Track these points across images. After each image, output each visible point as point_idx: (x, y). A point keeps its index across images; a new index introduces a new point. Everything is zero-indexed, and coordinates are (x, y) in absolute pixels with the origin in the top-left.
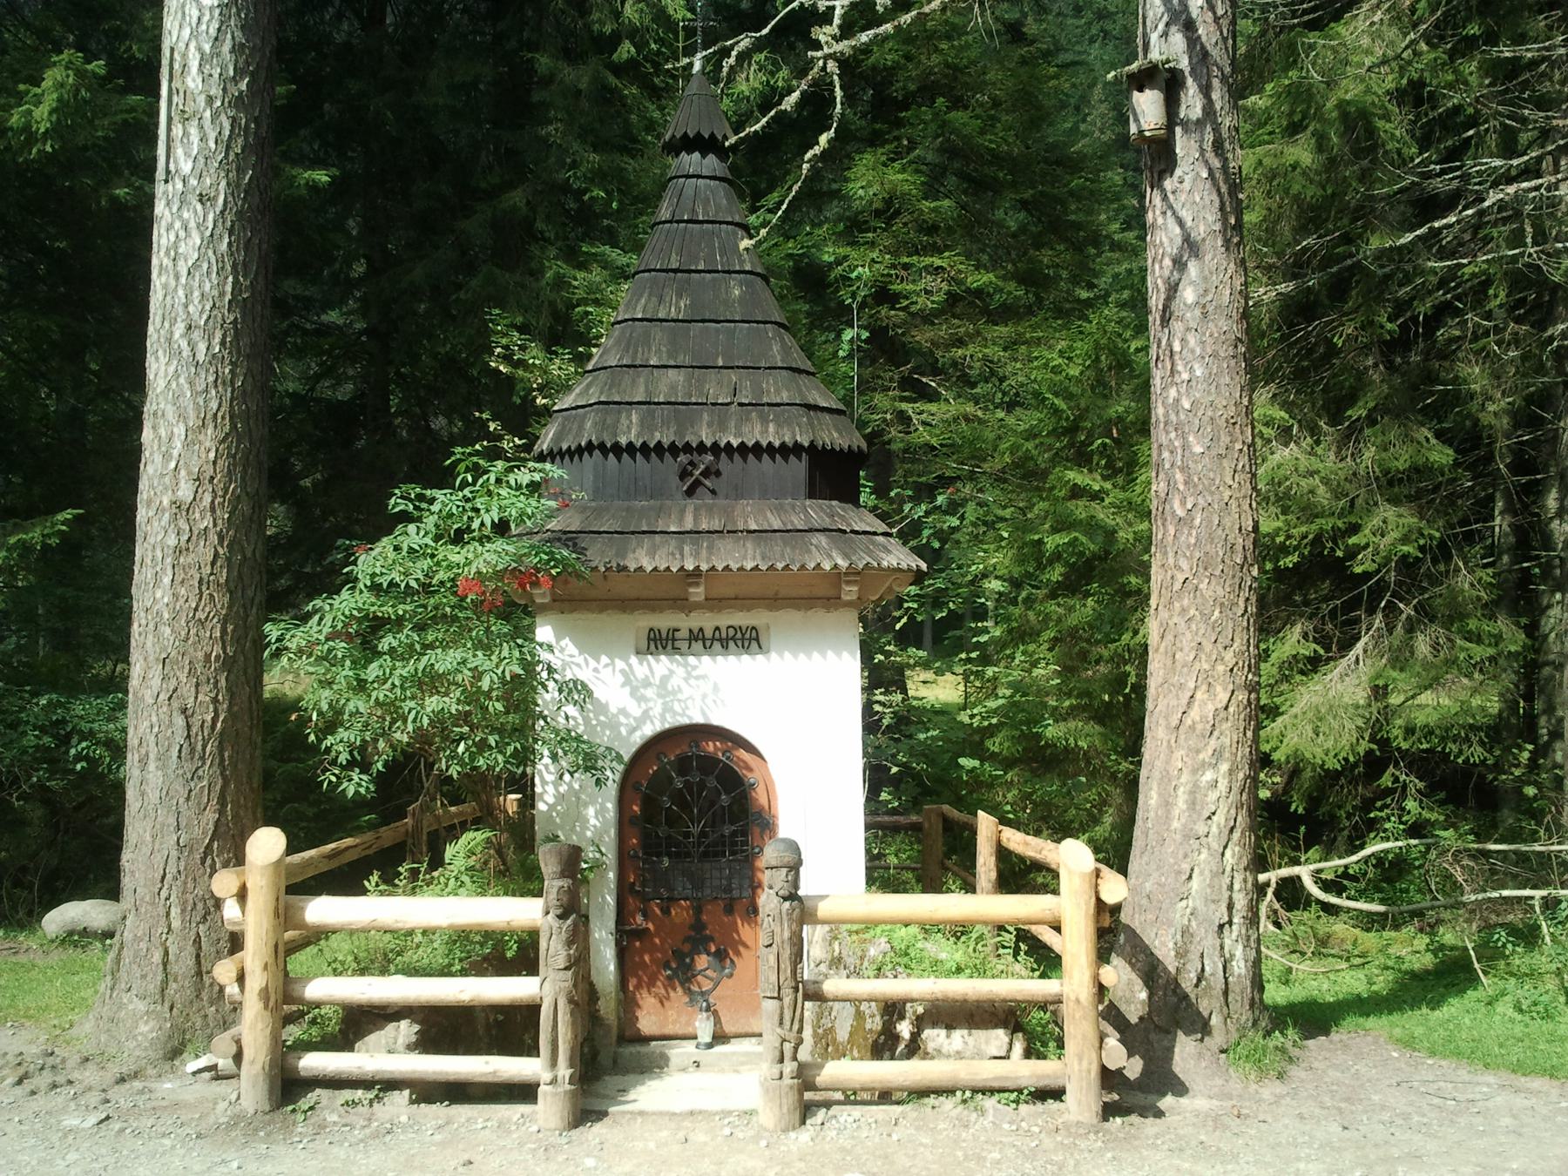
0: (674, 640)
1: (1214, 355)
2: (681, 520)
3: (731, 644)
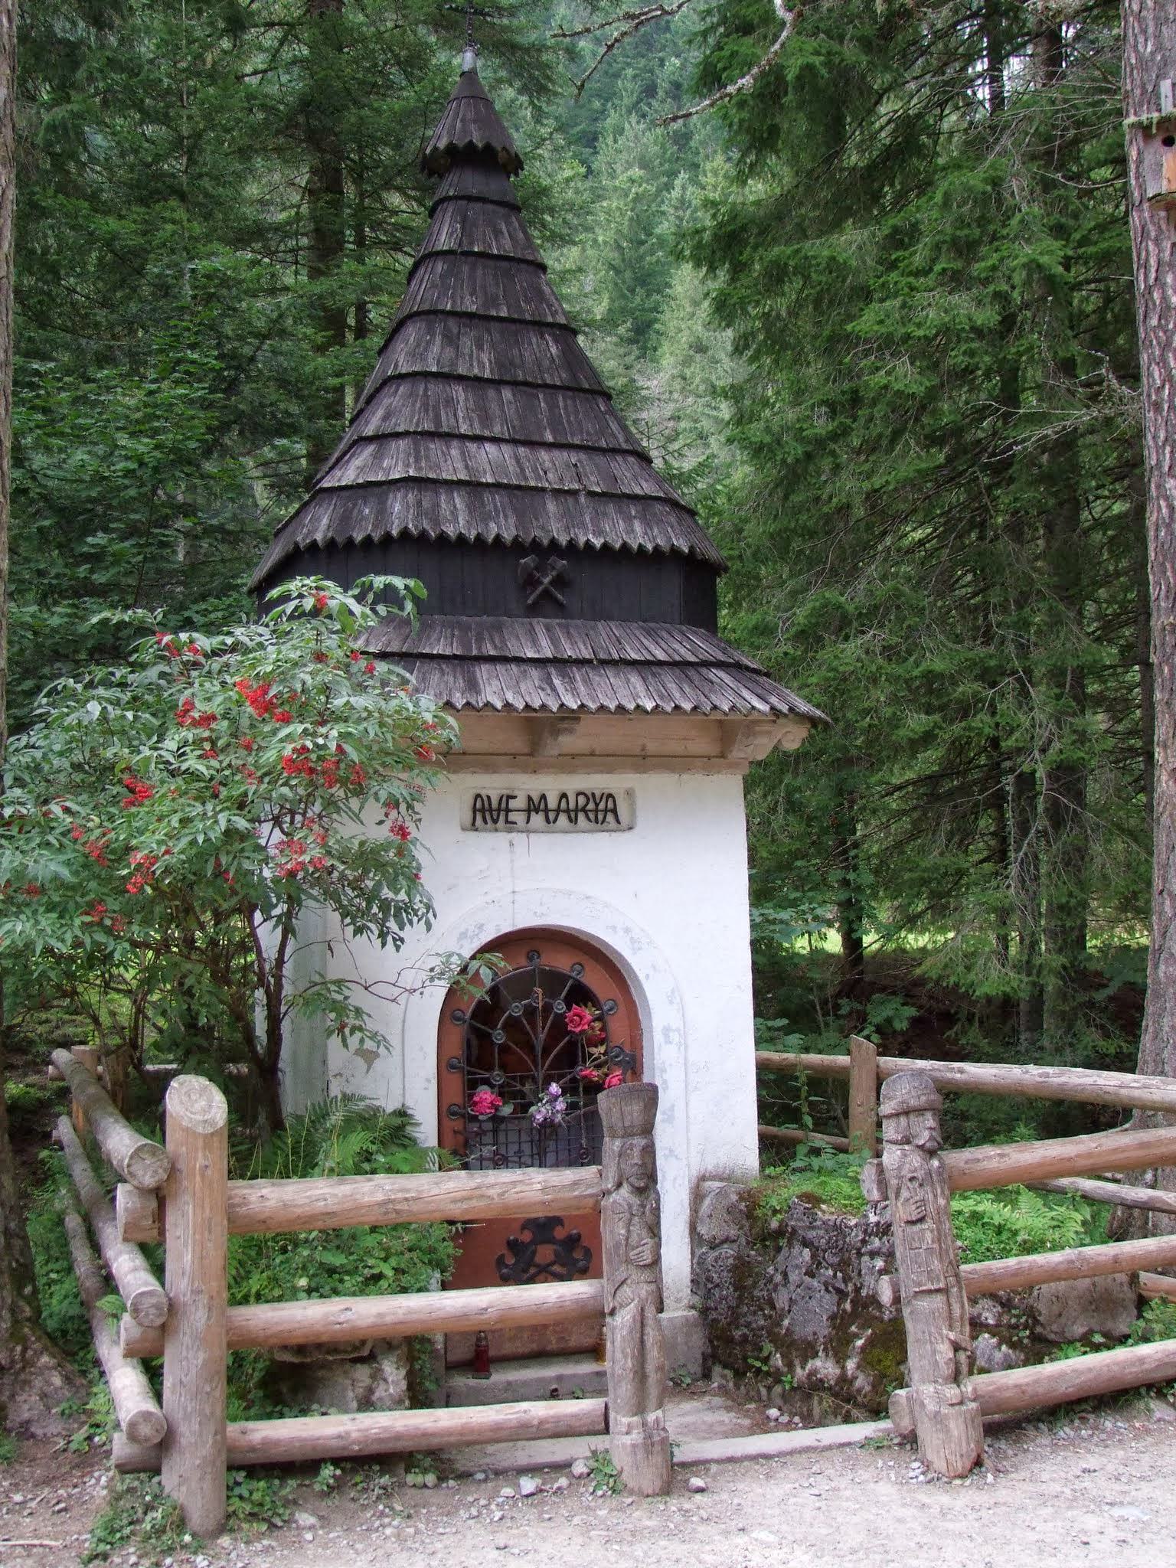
0: (508, 811)
3: (581, 816)
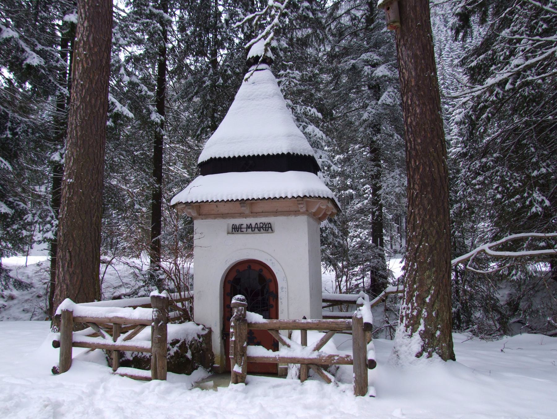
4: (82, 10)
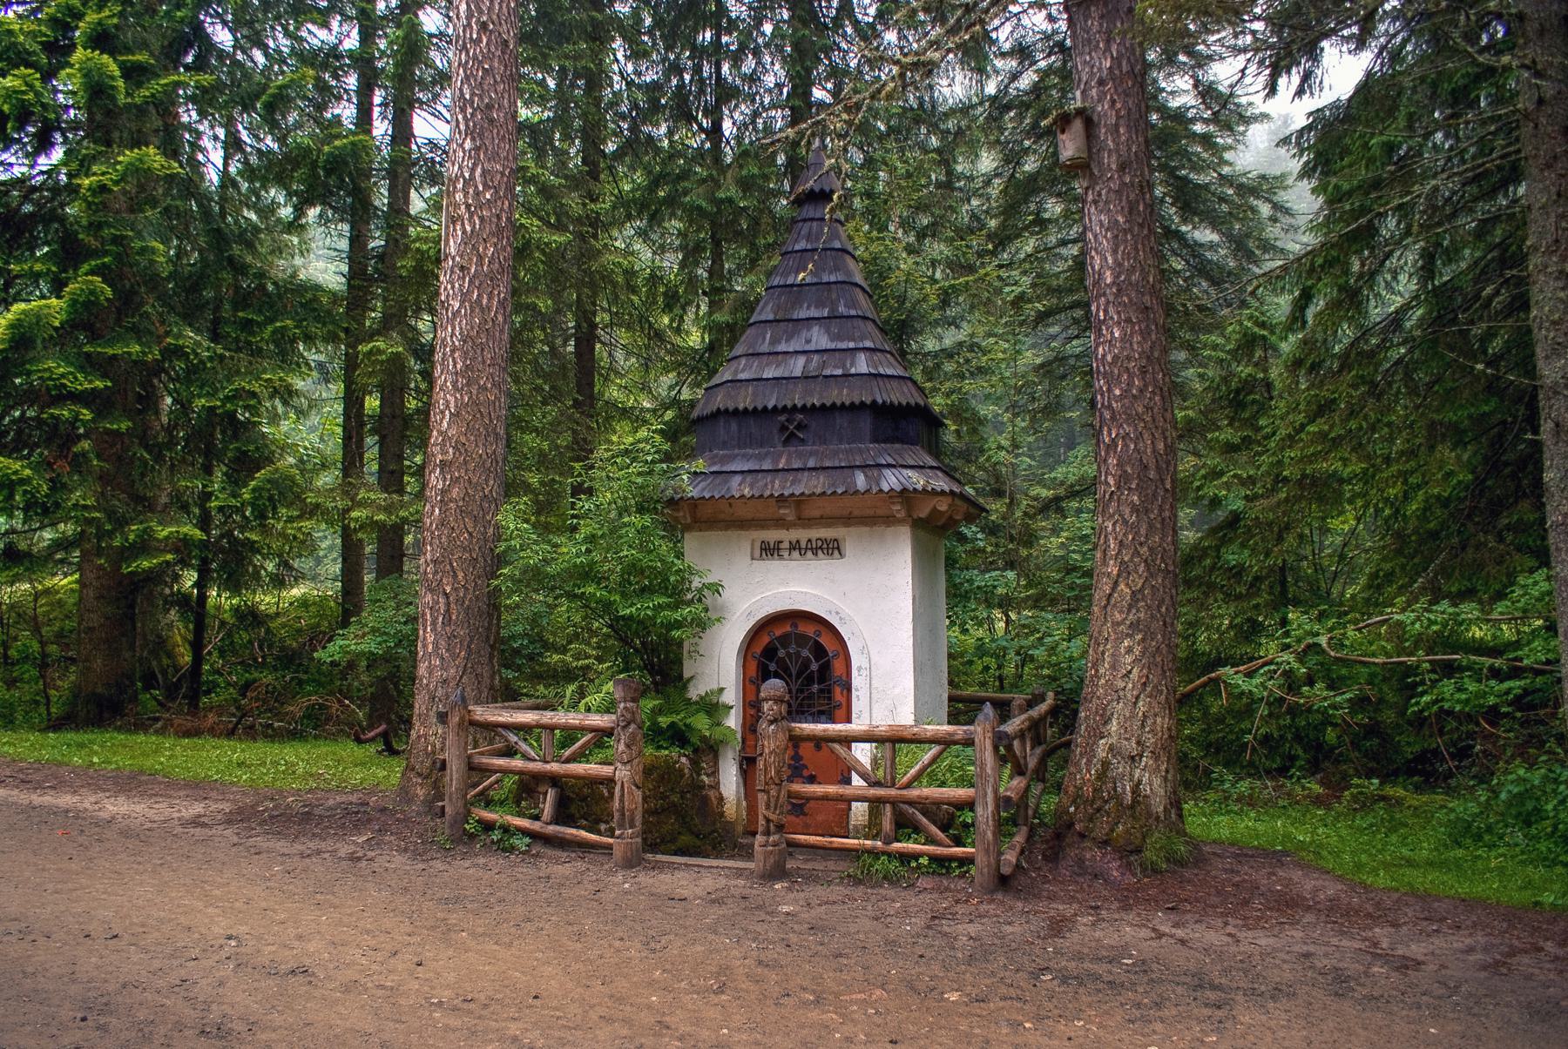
1: (1128, 320)
2: (777, 462)
4: (460, 117)
